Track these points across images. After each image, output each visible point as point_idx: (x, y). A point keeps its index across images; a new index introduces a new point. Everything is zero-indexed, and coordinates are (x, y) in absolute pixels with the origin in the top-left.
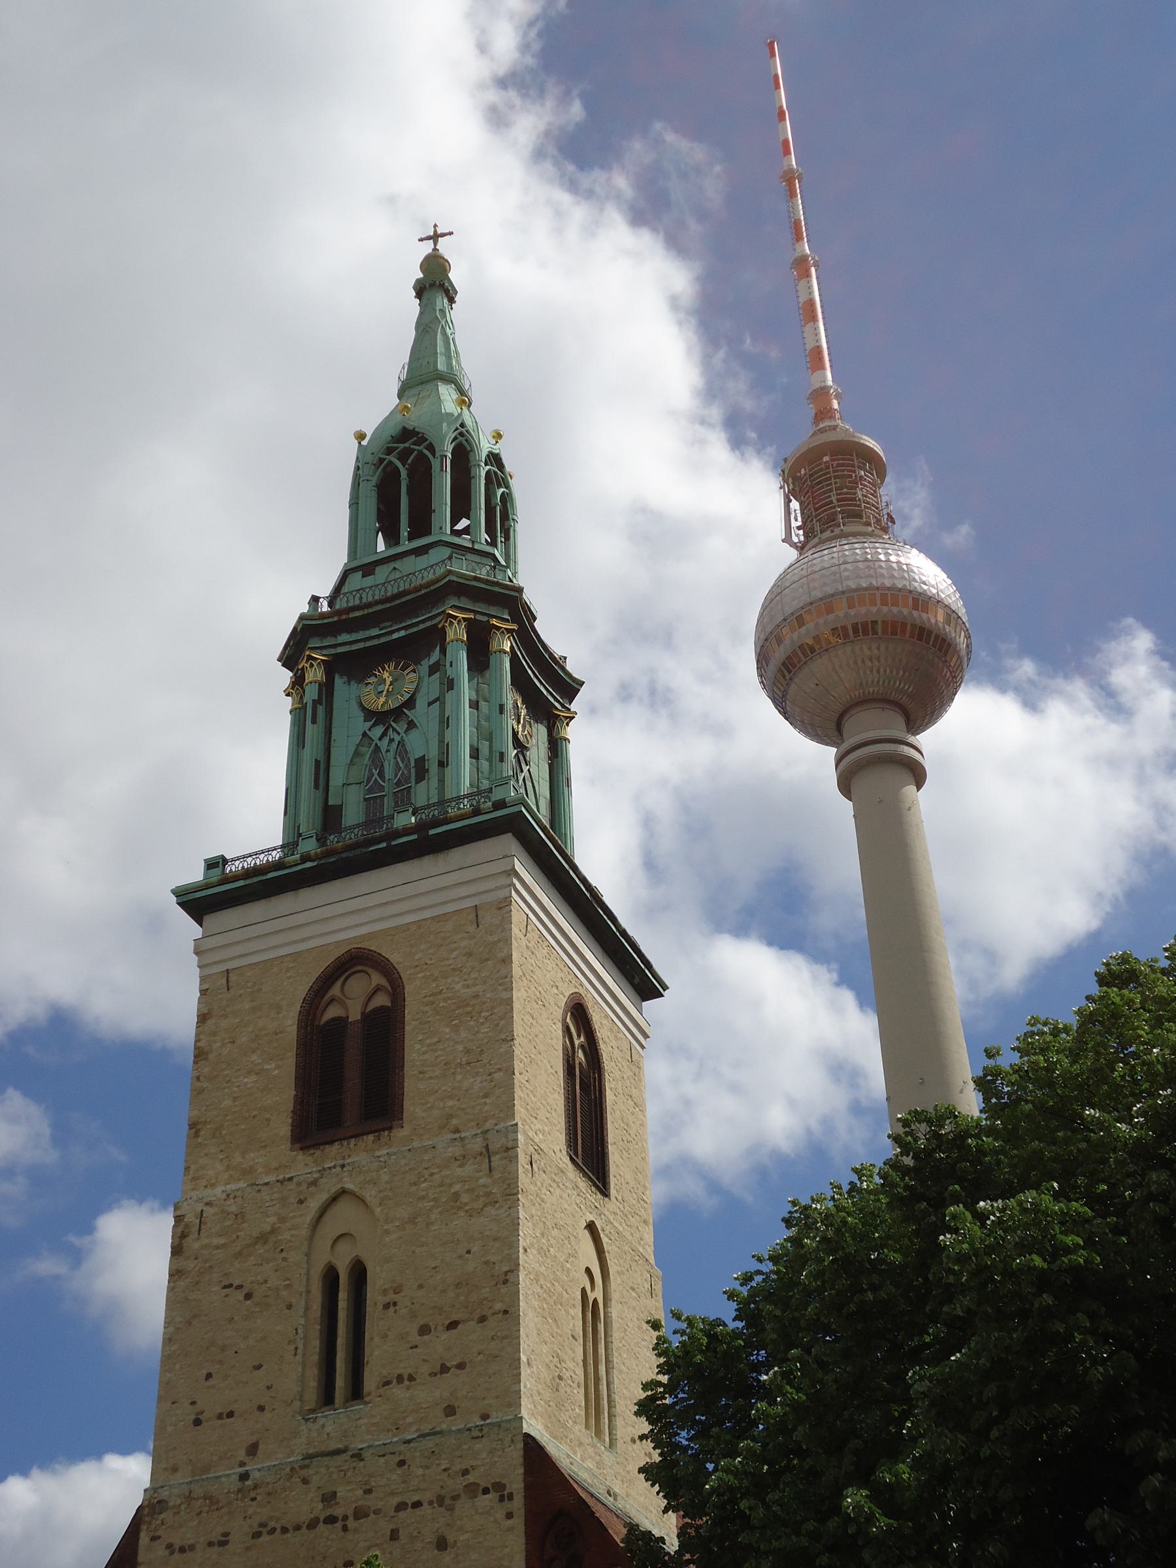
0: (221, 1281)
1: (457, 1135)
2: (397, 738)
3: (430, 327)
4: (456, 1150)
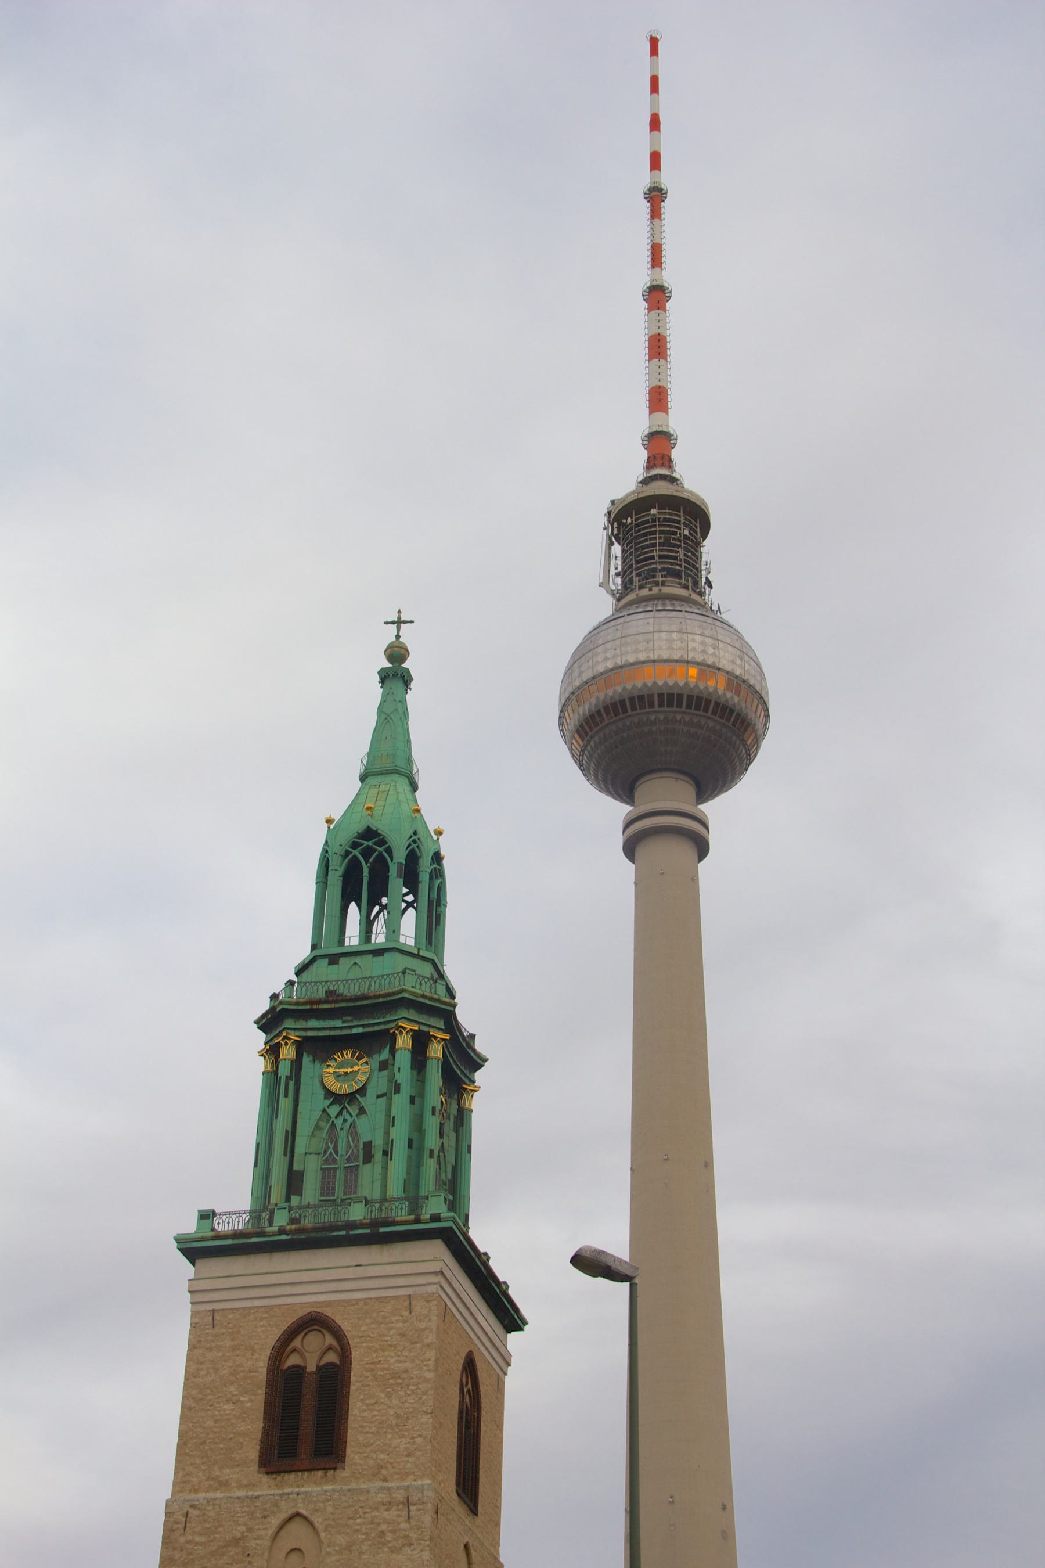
1: (385, 1484)
2: (350, 1120)
3: (391, 718)
4: (383, 1497)
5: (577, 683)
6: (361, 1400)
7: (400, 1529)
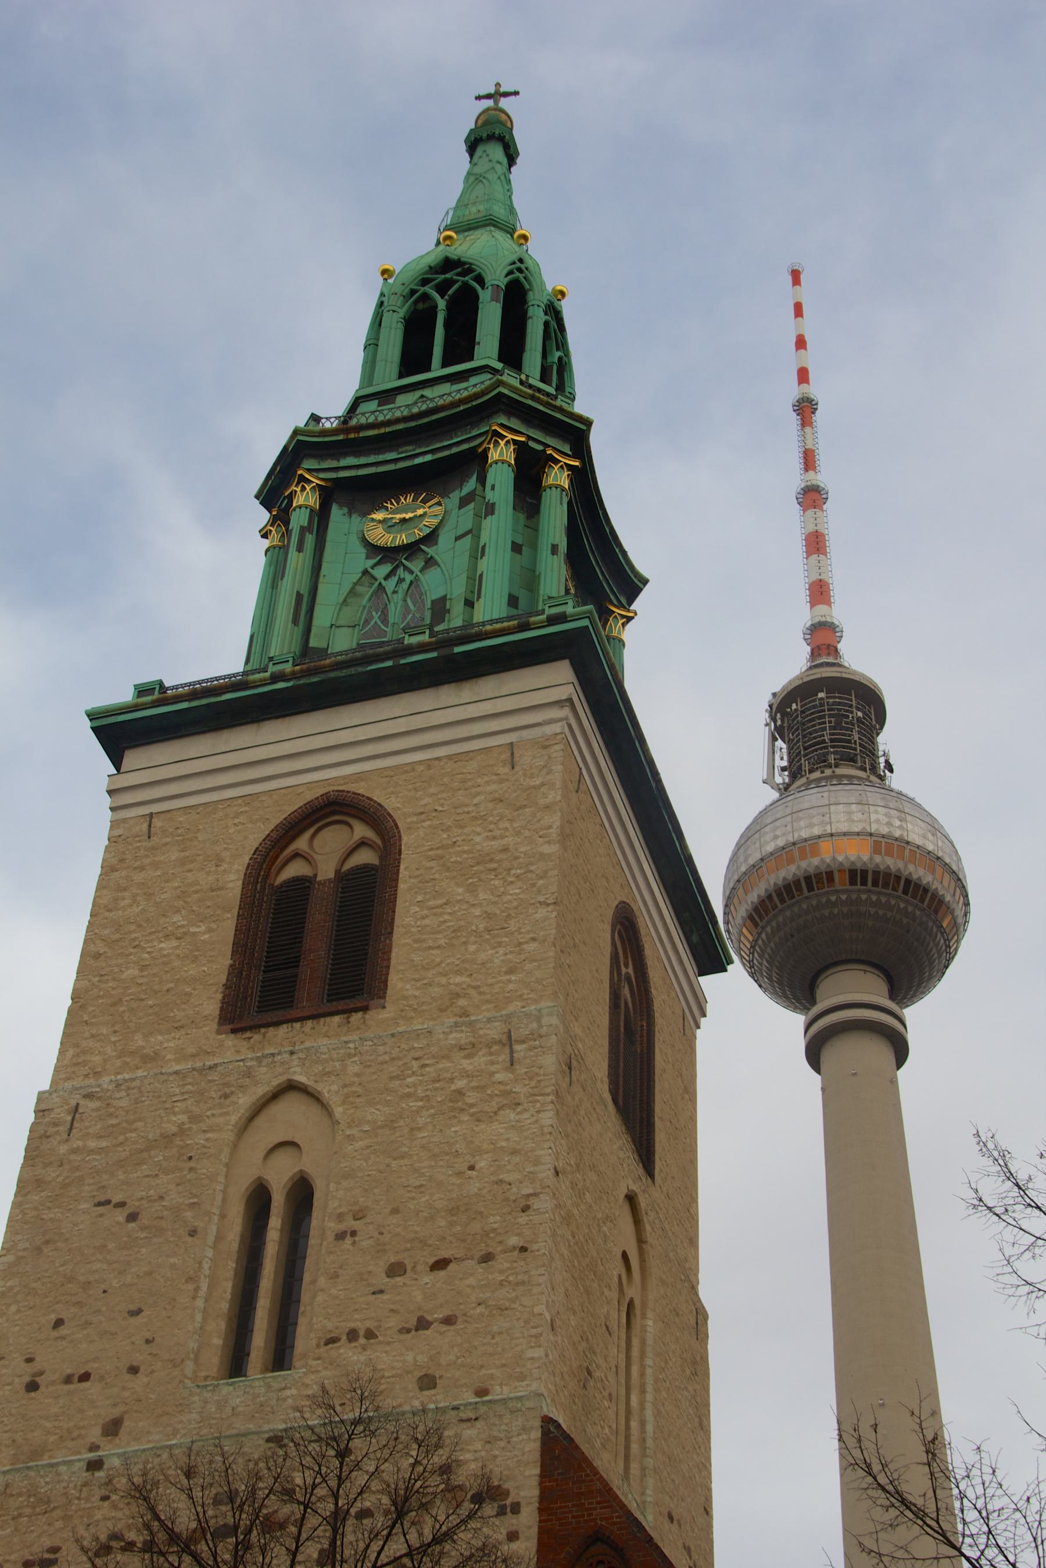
0: (94, 1196)
2: (409, 578)
4: (462, 1037)
5: (743, 869)
6: (418, 902)
7: (494, 1083)
